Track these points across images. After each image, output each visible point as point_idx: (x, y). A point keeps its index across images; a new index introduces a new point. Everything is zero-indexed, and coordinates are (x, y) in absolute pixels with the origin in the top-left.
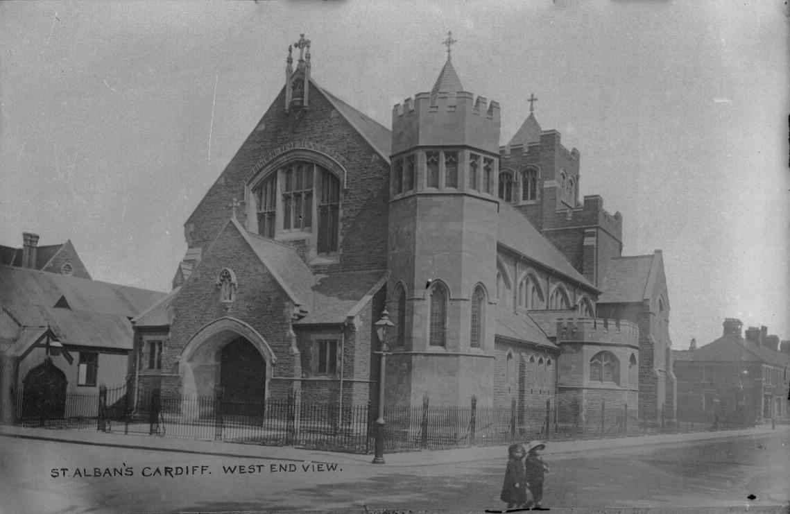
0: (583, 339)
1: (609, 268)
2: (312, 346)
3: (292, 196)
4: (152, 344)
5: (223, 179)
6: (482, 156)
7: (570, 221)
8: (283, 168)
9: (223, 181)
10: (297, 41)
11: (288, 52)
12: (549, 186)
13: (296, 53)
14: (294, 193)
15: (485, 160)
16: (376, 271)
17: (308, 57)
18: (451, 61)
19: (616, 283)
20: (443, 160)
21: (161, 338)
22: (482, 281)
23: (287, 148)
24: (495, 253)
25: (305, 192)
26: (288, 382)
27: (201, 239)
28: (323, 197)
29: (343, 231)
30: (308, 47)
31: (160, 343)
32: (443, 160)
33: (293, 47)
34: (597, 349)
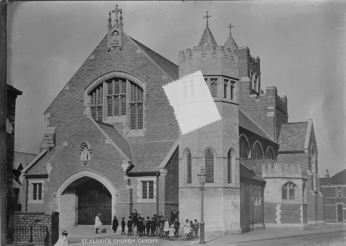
0: (308, 221)
1: (282, 130)
2: (138, 198)
4: (35, 185)
5: (68, 86)
6: (230, 80)
8: (106, 81)
10: (114, 9)
11: (108, 22)
13: (114, 16)
14: (114, 96)
16: (167, 141)
17: (121, 18)
18: (250, 54)
19: (287, 139)
21: (42, 181)
23: (109, 70)
24: (212, 98)
25: (121, 95)
29: (147, 118)
30: (121, 13)
31: (40, 184)
33: (111, 12)
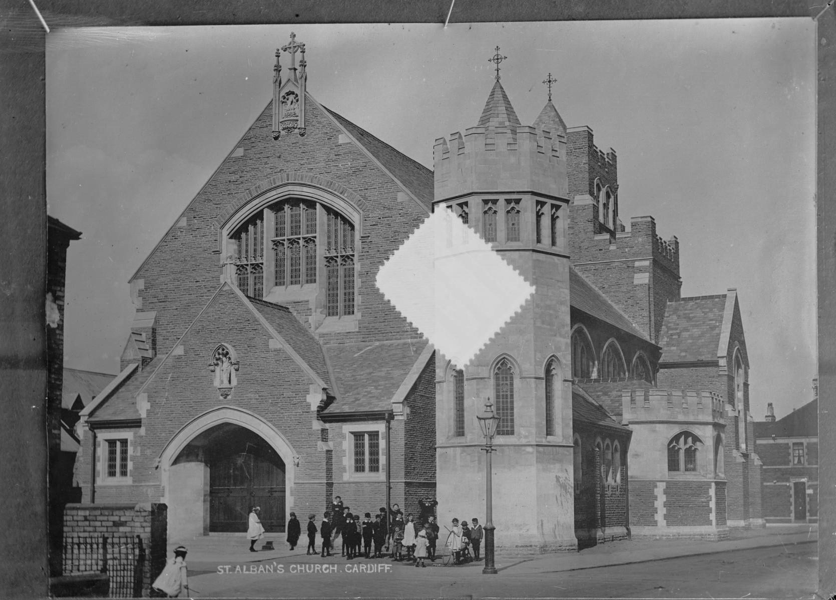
1: (666, 314)
3: (286, 243)
4: (112, 443)
7: (614, 251)
8: (271, 207)
9: (183, 223)
12: (580, 203)
15: (553, 206)
17: (303, 64)
19: (679, 335)
20: (501, 207)
22: (556, 354)
23: (276, 180)
26: (418, 484)
27: (155, 300)
28: (329, 243)
30: (303, 52)
31: (124, 442)
32: (501, 207)
33: (281, 51)
34: (676, 430)
